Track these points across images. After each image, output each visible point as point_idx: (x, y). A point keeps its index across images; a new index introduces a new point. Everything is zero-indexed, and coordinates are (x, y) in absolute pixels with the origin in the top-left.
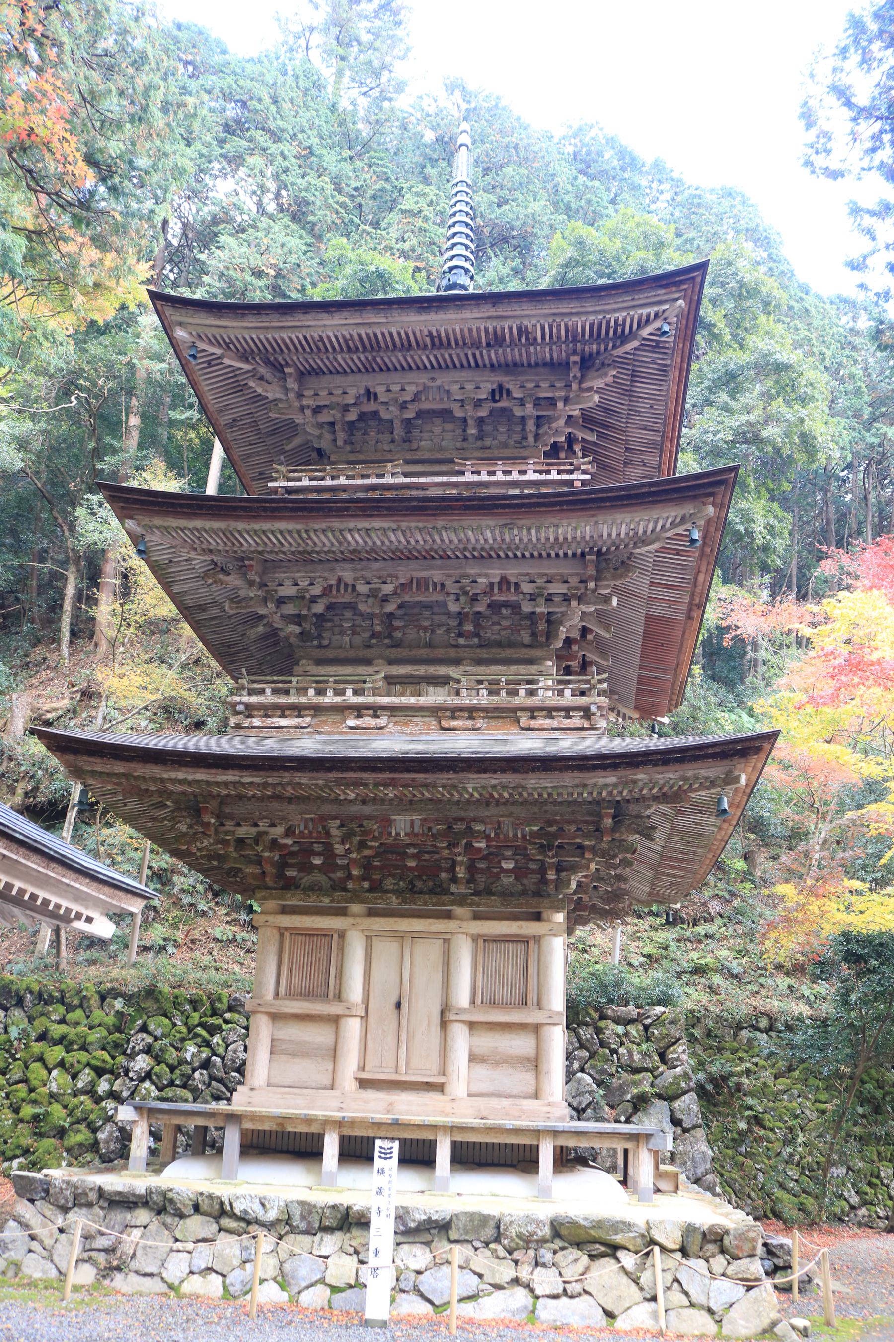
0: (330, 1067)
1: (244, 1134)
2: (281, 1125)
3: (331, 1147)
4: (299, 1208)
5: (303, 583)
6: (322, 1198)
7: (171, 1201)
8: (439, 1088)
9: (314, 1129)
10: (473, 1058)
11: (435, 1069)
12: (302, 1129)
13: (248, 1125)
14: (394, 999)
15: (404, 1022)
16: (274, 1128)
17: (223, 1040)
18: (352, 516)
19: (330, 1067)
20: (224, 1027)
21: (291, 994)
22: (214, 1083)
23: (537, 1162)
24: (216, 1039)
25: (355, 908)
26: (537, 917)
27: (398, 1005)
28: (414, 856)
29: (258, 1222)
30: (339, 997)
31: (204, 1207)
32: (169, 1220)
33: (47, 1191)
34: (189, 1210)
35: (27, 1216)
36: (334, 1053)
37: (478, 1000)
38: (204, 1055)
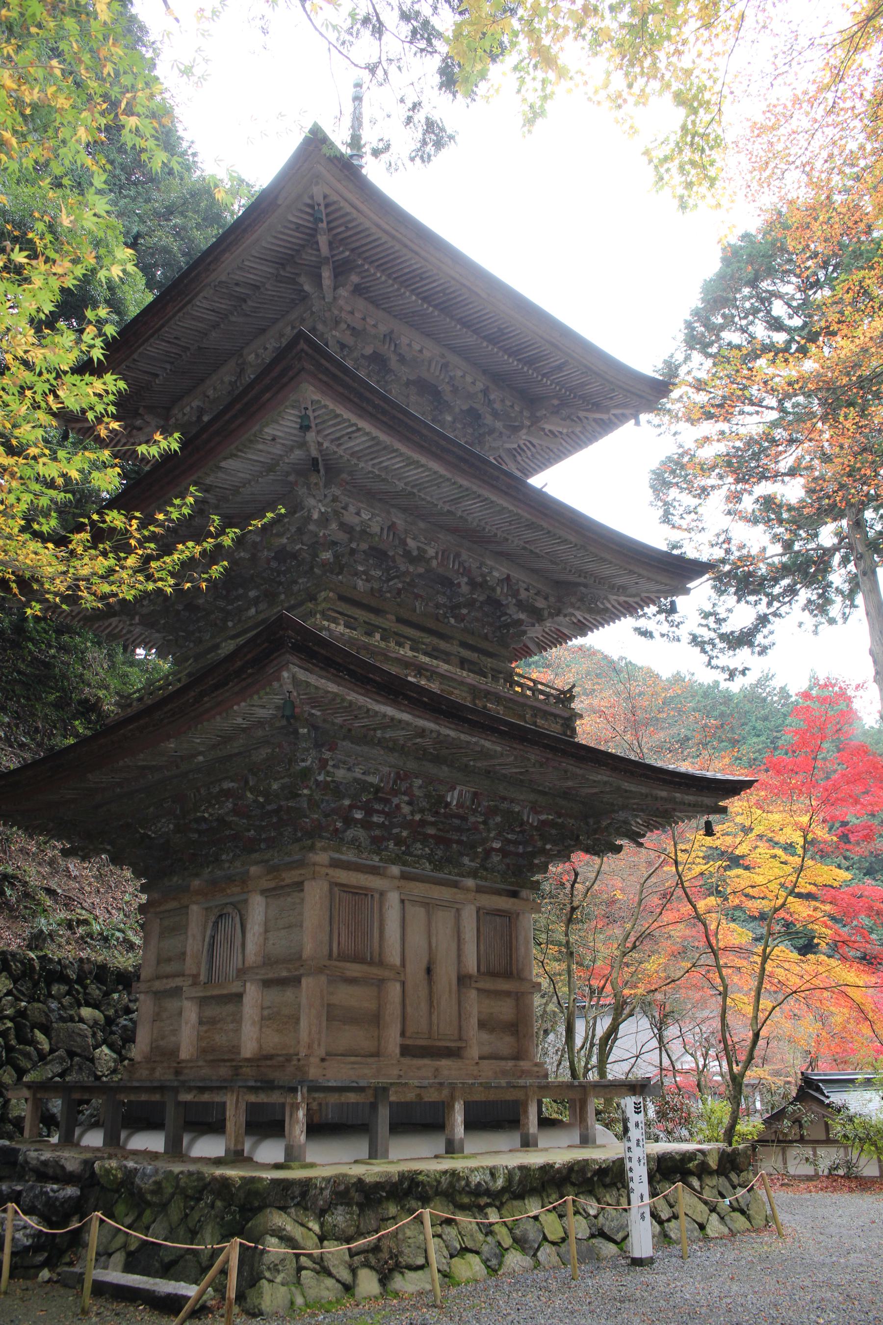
6: (534, 1159)
7: (418, 1184)
14: (424, 965)
26: (514, 894)
29: (488, 1193)
33: (304, 1194)
35: (288, 1228)
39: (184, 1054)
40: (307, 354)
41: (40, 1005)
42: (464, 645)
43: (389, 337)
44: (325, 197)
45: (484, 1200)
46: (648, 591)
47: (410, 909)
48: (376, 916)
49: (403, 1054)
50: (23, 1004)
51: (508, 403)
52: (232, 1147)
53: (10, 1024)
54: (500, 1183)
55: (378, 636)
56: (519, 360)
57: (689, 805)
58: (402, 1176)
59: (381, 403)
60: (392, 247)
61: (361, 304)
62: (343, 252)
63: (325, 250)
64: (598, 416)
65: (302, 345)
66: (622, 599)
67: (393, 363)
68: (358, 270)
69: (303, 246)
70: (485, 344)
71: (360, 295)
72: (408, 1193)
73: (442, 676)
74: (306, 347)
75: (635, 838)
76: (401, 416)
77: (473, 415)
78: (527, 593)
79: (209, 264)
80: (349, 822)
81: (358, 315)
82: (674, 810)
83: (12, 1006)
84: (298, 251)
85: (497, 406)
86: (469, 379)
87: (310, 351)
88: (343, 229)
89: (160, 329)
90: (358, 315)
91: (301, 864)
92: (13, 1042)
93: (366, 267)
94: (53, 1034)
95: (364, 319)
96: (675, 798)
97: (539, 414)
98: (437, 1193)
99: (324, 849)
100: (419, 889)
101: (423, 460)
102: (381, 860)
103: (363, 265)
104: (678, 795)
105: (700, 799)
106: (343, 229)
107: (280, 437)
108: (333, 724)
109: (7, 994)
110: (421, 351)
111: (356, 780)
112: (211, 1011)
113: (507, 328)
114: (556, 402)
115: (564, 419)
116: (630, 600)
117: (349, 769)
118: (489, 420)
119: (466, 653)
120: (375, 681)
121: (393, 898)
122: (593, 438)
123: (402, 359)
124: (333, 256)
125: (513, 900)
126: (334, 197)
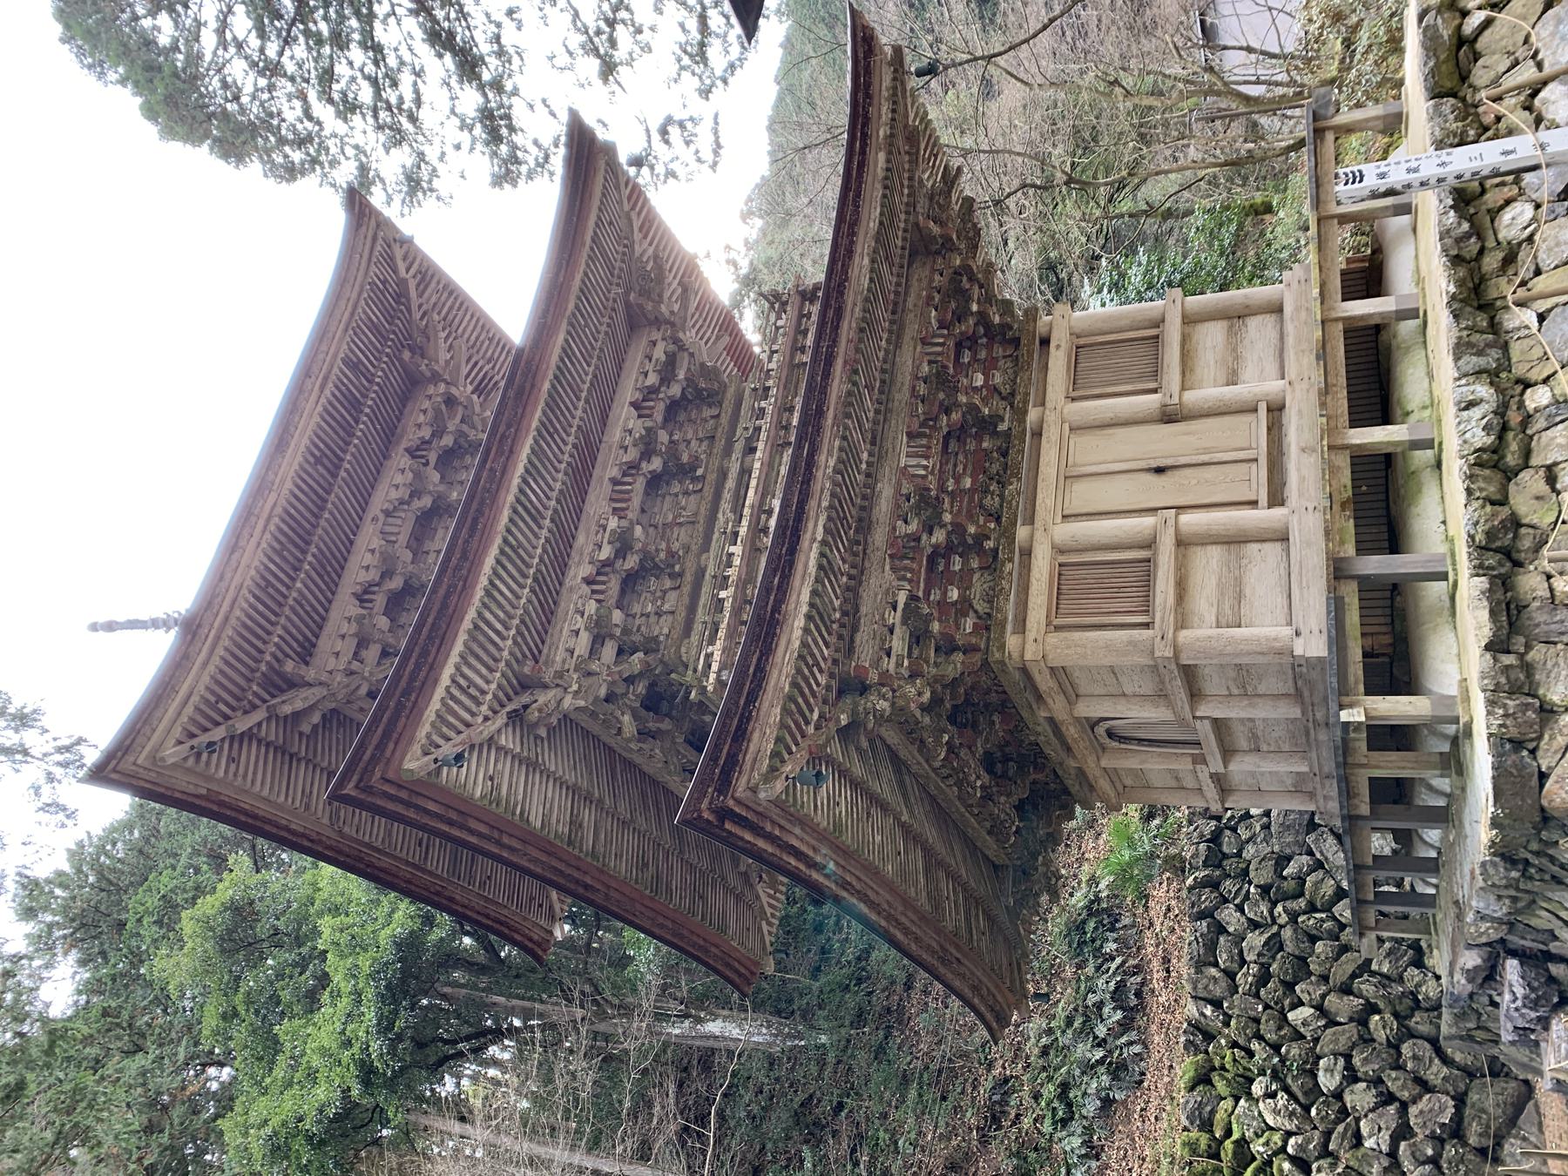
0: (1255, 547)
1: (1362, 549)
2: (1343, 506)
3: (1377, 565)
4: (1466, 358)
5: (580, 623)
6: (1442, 328)
8: (1276, 410)
9: (1343, 461)
10: (1232, 379)
11: (1250, 418)
12: (1346, 477)
13: (1350, 549)
15: (1183, 461)
17: (1258, 1136)
18: (503, 473)
19: (1253, 548)
20: (1236, 1136)
21: (1147, 606)
22: (1331, 1147)
23: (1397, 779)
24: (1257, 1147)
25: (1022, 532)
26: (1045, 342)
27: (1160, 470)
28: (958, 480)
29: (1501, 411)
30: (1150, 544)
31: (1492, 490)
32: (1526, 544)
33: (1518, 744)
34: (1504, 512)
36: (1235, 540)
37: (1152, 385)
40: (360, 780)
42: (728, 452)
43: (363, 597)
45: (1514, 418)
46: (620, 202)
47: (1077, 502)
48: (1129, 388)
50: (1252, 890)
51: (422, 418)
53: (1279, 908)
55: (723, 594)
57: (894, 111)
58: (1480, 569)
59: (413, 660)
60: (231, 638)
61: (325, 644)
62: (255, 693)
63: (259, 715)
64: (413, 293)
65: (349, 789)
66: (637, 236)
67: (396, 583)
68: (276, 665)
70: (343, 474)
73: (763, 496)
74: (352, 785)
75: (951, 178)
76: (425, 631)
77: (448, 459)
78: (650, 374)
79: (312, 841)
80: (964, 606)
82: (906, 126)
84: (268, 745)
85: (426, 433)
86: (399, 479)
87: (355, 778)
89: (414, 865)
91: (1024, 671)
92: (1302, 903)
93: (268, 658)
94: (1288, 851)
95: (343, 637)
96: (886, 137)
99: (1002, 647)
100: (1046, 497)
101: (483, 581)
102: (1011, 560)
103: (268, 663)
104: (881, 133)
105: (885, 94)
107: (486, 770)
108: (828, 688)
109: (1242, 912)
110: (373, 551)
111: (904, 622)
114: (406, 355)
115: (428, 339)
116: (636, 225)
118: (447, 441)
119: (739, 447)
120: (759, 660)
122: (450, 290)
124: (265, 701)
125: (1053, 344)
126: (177, 732)
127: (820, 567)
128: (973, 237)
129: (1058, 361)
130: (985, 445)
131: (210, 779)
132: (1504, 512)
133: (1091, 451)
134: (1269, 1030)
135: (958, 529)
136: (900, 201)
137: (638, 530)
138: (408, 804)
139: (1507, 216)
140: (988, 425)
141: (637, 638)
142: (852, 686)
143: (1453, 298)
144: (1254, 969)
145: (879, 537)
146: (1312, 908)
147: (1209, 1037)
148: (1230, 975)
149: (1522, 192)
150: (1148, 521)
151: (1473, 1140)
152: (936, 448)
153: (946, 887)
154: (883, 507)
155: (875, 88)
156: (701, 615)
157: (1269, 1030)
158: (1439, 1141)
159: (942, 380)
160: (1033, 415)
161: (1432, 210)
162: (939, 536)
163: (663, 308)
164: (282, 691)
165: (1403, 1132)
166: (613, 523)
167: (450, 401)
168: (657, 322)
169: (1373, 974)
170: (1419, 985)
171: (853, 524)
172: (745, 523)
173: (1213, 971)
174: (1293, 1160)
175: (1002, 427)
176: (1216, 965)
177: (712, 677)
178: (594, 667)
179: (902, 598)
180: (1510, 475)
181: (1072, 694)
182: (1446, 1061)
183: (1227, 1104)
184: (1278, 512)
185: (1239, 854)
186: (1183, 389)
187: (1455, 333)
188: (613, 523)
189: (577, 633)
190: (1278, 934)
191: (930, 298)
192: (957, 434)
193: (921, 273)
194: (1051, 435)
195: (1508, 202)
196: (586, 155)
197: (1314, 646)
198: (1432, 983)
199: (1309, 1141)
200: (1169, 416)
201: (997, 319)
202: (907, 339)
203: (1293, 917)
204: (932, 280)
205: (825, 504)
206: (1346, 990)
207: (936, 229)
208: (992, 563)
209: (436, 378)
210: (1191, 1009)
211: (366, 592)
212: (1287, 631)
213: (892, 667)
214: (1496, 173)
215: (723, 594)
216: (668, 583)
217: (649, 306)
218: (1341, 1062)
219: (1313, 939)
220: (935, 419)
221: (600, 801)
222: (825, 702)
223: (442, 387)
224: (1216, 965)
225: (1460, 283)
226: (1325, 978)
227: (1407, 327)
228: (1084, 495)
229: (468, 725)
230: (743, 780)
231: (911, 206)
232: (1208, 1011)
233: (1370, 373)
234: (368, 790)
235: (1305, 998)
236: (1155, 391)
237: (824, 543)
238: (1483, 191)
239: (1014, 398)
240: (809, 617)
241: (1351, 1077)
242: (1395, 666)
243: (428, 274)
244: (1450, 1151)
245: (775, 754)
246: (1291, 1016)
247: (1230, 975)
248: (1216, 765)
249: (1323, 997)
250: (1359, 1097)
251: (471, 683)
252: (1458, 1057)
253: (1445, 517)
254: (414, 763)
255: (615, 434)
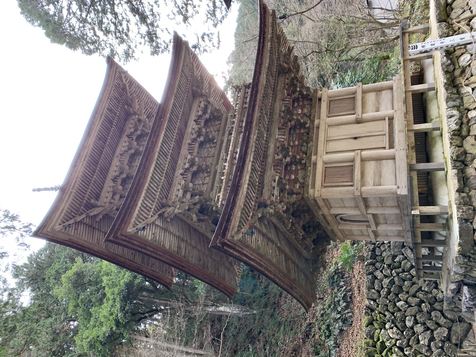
2: (412, 148)
3: (423, 166)
5: (179, 187)
6: (442, 93)
7: (457, 156)
8: (391, 119)
9: (412, 135)
11: (383, 122)
12: (413, 139)
13: (414, 162)
15: (363, 135)
16: (415, 153)
17: (387, 340)
19: (384, 161)
20: (381, 340)
21: (352, 180)
24: (387, 344)
25: (313, 158)
26: (320, 100)
27: (355, 138)
28: (294, 142)
29: (461, 118)
30: (353, 161)
31: (458, 143)
32: (469, 159)
33: (467, 220)
34: (462, 149)
36: (379, 159)
37: (353, 112)
38: (396, 349)
39: (401, 229)
41: (385, 259)
42: (223, 135)
43: (114, 180)
44: (60, 224)
45: (465, 120)
46: (190, 59)
49: (393, 148)
50: (385, 266)
52: (442, 229)
53: (394, 271)
54: (455, 112)
55: (222, 178)
56: (111, 127)
57: (273, 30)
58: (454, 167)
61: (103, 194)
63: (84, 216)
66: (195, 69)
67: (124, 176)
69: (84, 224)
71: (100, 195)
72: (463, 162)
75: (290, 50)
77: (139, 138)
81: (107, 195)
82: (276, 34)
83: (386, 270)
86: (124, 144)
88: (72, 213)
90: (107, 195)
92: (400, 270)
94: (396, 254)
95: (108, 192)
96: (270, 38)
97: (133, 112)
98: (461, 146)
99: (308, 193)
104: (269, 37)
105: (270, 24)
106: (72, 213)
109: (382, 272)
110: (117, 166)
112: (382, 221)
113: (98, 137)
116: (195, 66)
117: (274, 188)
119: (227, 133)
121: (327, 157)
123: (121, 173)
126: (59, 221)
127: (252, 169)
128: (298, 68)
129: (324, 105)
130: (302, 131)
131: (69, 235)
132: (462, 149)
133: (334, 133)
134: (391, 308)
135: (294, 157)
136: (275, 57)
137: (197, 159)
138: (129, 242)
139: (462, 58)
140: (303, 125)
141: (197, 191)
142: (262, 205)
143: (446, 84)
144: (386, 290)
145: (270, 160)
146: (404, 271)
147: (372, 310)
148: (379, 292)
149: (467, 51)
150: (352, 154)
151: (454, 341)
152: (287, 133)
153: (292, 266)
154: (271, 150)
155: (267, 23)
156: (216, 184)
157: (391, 308)
158: (443, 342)
159: (289, 112)
160: (316, 122)
161: (439, 57)
162: (288, 159)
163: (203, 91)
164: (90, 209)
165: (432, 339)
166: (189, 157)
167: (139, 120)
168: (202, 95)
169: (422, 291)
170: (436, 294)
171: (262, 156)
172: (229, 156)
173: (373, 291)
174: (399, 348)
175: (307, 126)
176: (374, 289)
177: (220, 203)
178: (184, 200)
179: (277, 178)
180: (464, 138)
181: (330, 207)
182: (445, 317)
183: (378, 331)
184: (392, 150)
185: (381, 255)
186: (362, 113)
187: (446, 95)
188: (189, 157)
189: (179, 190)
190: (393, 279)
191: (284, 87)
192: (293, 128)
193: (282, 79)
194: (322, 128)
195: (462, 54)
196: (179, 45)
197: (404, 191)
198: (441, 294)
199: (403, 342)
200: (358, 122)
201: (305, 93)
202: (278, 99)
203: (398, 274)
204: (285, 81)
205: (253, 150)
206: (414, 296)
207: (286, 66)
208: (304, 167)
209: (135, 114)
210: (367, 302)
211: (115, 178)
212: (395, 187)
213: (274, 199)
214: (459, 45)
215: (222, 178)
216: (206, 175)
217: (199, 91)
218: (413, 318)
219: (404, 281)
220: (287, 123)
221: (186, 241)
222: (254, 210)
223: (137, 116)
224: (374, 289)
225: (448, 79)
226: (408, 293)
227: (431, 93)
228: (332, 146)
229: (146, 218)
230: (230, 234)
231: (278, 59)
232: (372, 303)
233: (420, 107)
234: (117, 238)
235: (402, 298)
236: (354, 114)
237: (253, 162)
238: (455, 51)
239: (310, 117)
240: (249, 185)
241: (416, 322)
242: (428, 197)
243: (132, 82)
244: (447, 345)
245: (239, 226)
246: (397, 304)
247: (379, 292)
248: (374, 228)
249: (407, 298)
250: (419, 328)
251: (147, 205)
252: (449, 316)
253: (444, 151)
254: (130, 230)
255: (189, 130)
